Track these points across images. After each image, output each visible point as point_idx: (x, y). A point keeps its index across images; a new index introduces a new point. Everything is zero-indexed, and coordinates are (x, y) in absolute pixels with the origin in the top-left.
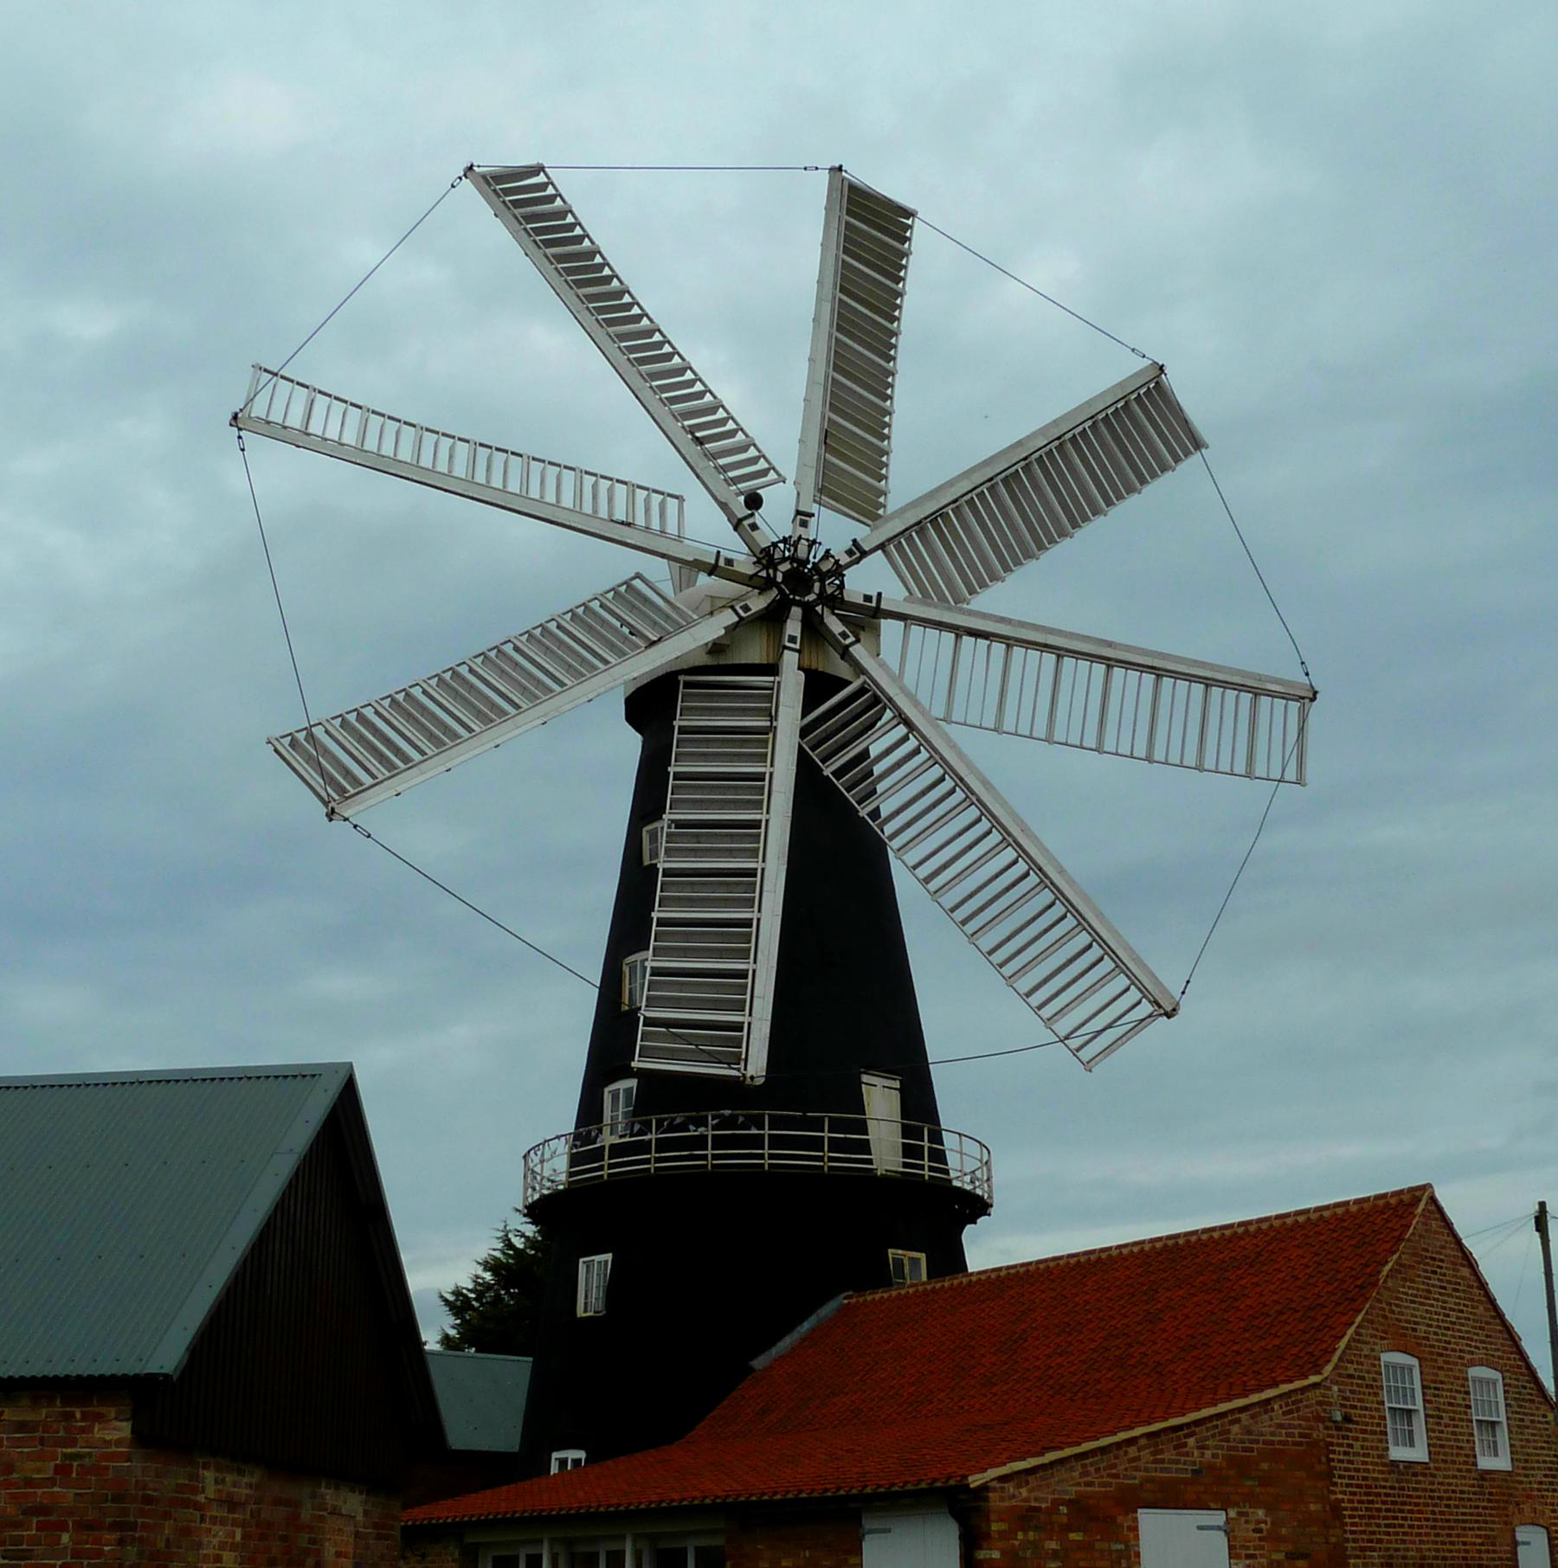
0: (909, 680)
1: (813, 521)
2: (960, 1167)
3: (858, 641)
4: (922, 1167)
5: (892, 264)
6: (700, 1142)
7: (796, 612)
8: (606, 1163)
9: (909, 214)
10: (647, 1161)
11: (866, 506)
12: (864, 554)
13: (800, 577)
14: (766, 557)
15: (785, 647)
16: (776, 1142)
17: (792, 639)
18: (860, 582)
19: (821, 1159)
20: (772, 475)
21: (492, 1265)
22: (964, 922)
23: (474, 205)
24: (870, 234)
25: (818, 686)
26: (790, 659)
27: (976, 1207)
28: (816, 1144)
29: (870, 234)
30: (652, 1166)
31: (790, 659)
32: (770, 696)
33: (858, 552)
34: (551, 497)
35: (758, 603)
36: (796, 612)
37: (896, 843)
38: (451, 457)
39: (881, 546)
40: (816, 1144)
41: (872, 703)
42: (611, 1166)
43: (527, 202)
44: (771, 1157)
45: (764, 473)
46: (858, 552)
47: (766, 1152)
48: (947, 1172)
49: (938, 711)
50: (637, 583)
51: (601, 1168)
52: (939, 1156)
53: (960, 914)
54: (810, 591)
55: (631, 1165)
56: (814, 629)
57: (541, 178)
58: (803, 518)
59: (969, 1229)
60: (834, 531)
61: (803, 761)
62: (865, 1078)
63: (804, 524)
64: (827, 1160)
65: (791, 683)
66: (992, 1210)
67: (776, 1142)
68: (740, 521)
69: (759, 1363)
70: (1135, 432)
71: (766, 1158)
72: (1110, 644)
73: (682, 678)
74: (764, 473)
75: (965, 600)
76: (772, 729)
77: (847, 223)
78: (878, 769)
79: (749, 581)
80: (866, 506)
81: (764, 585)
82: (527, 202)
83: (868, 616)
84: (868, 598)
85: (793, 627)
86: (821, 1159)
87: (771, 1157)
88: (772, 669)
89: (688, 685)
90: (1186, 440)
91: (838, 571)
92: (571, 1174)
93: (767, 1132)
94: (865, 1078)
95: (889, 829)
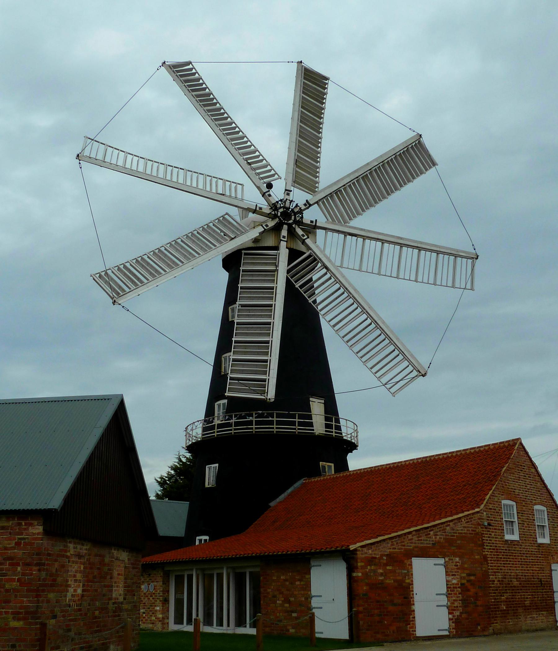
0: (327, 252)
2: (347, 432)
4: (332, 432)
5: (321, 98)
6: (251, 423)
7: (285, 227)
8: (216, 430)
9: (327, 79)
10: (231, 430)
11: (310, 186)
12: (310, 205)
13: (287, 214)
15: (281, 240)
17: (284, 237)
18: (308, 216)
19: (295, 429)
20: (276, 176)
24: (312, 86)
25: (294, 254)
26: (283, 245)
27: (352, 446)
28: (293, 423)
30: (233, 432)
31: (283, 245)
32: (276, 258)
33: (308, 205)
35: (271, 224)
36: (285, 227)
40: (293, 423)
42: (218, 432)
44: (277, 428)
46: (308, 205)
47: (275, 426)
48: (341, 434)
49: (338, 263)
50: (226, 216)
51: (214, 432)
52: (339, 428)
56: (292, 233)
57: (190, 66)
58: (288, 192)
59: (350, 454)
60: (299, 197)
61: (288, 281)
63: (288, 194)
64: (297, 429)
65: (284, 253)
66: (358, 448)
67: (278, 423)
69: (272, 504)
71: (275, 429)
72: (401, 238)
73: (243, 252)
78: (316, 285)
79: (268, 215)
81: (274, 217)
85: (284, 233)
86: (295, 429)
87: (277, 428)
88: (276, 248)
90: (430, 162)
91: (301, 212)
92: (203, 435)
93: (275, 419)
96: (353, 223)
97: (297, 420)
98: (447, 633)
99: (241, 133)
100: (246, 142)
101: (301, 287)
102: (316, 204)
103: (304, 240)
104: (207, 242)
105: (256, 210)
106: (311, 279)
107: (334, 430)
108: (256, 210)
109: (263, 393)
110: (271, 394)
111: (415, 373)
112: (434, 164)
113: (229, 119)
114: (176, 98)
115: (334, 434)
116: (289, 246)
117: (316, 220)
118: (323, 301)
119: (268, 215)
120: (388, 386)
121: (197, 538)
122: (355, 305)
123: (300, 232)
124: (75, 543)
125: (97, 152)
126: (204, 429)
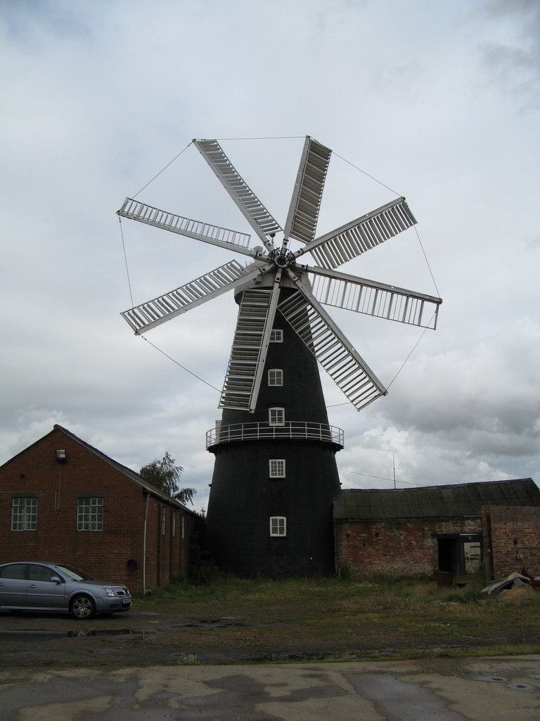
0: (314, 293)
4: (319, 436)
5: (323, 166)
7: (280, 270)
8: (258, 434)
9: (331, 151)
11: (306, 236)
12: (303, 253)
13: (282, 260)
14: (272, 254)
18: (300, 261)
20: (279, 229)
21: (144, 470)
22: (335, 379)
23: (194, 150)
24: (316, 159)
25: (285, 292)
27: (339, 447)
29: (316, 159)
31: (277, 286)
32: (268, 297)
33: (302, 252)
34: (317, 354)
35: (268, 268)
36: (280, 270)
37: (320, 359)
41: (303, 299)
43: (210, 150)
45: (277, 228)
46: (302, 252)
47: (307, 433)
49: (323, 301)
50: (233, 263)
52: (329, 433)
53: (344, 389)
55: (283, 435)
56: (285, 275)
57: (216, 143)
59: (338, 452)
60: (295, 245)
61: (277, 312)
63: (285, 244)
65: (276, 292)
67: (293, 430)
70: (397, 216)
71: (306, 436)
74: (277, 228)
76: (268, 307)
78: (313, 331)
79: (266, 260)
80: (306, 236)
81: (272, 262)
82: (210, 150)
83: (305, 270)
84: (303, 266)
88: (271, 288)
90: (412, 220)
91: (294, 258)
93: (320, 429)
95: (317, 354)
97: (306, 428)
99: (270, 217)
100: (274, 225)
101: (290, 320)
106: (309, 326)
107: (321, 435)
109: (247, 406)
111: (377, 393)
112: (415, 222)
113: (252, 195)
114: (198, 159)
115: (321, 438)
116: (282, 285)
118: (318, 345)
119: (266, 260)
120: (354, 403)
121: (271, 518)
122: (333, 336)
123: (292, 274)
125: (133, 209)
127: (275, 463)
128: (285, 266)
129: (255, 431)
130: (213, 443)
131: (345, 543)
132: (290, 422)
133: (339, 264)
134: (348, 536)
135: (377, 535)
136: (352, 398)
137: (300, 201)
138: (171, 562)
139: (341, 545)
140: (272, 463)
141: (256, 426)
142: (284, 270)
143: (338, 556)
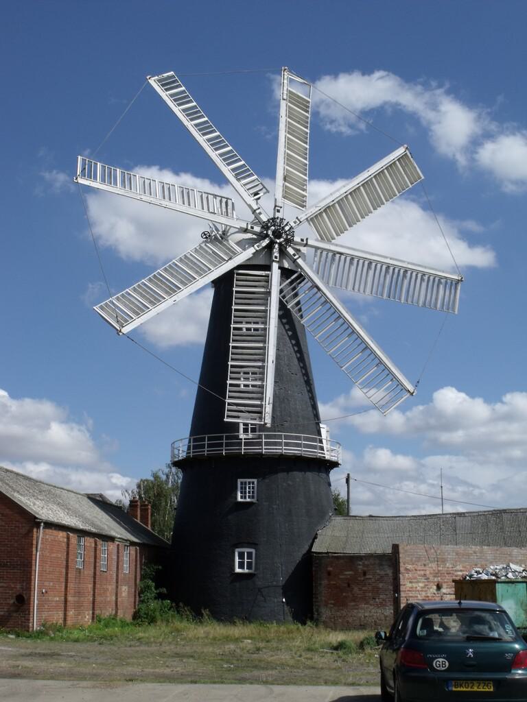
1: (281, 210)
3: (300, 257)
15: (273, 261)
16: (267, 444)
17: (276, 257)
25: (285, 273)
26: (275, 266)
28: (280, 444)
32: (267, 280)
38: (328, 337)
39: (317, 248)
40: (280, 444)
54: (279, 238)
58: (277, 209)
61: (281, 302)
62: (170, 543)
65: (276, 272)
67: (267, 444)
68: (255, 211)
73: (235, 271)
75: (334, 239)
76: (269, 293)
77: (359, 384)
85: (276, 253)
88: (268, 268)
89: (238, 274)
94: (170, 543)
96: (338, 240)
98: (387, 398)
102: (314, 249)
103: (296, 259)
104: (198, 263)
105: (247, 229)
108: (247, 229)
110: (268, 420)
117: (307, 239)
124: (121, 593)
126: (187, 453)
127: (245, 483)
128: (282, 240)
129: (221, 445)
130: (182, 455)
131: (325, 582)
132: (224, 435)
133: (338, 235)
134: (329, 573)
135: (365, 574)
136: (258, 402)
137: (346, 197)
138: (117, 599)
139: (320, 584)
140: (242, 483)
141: (221, 438)
142: (280, 244)
143: (317, 598)
